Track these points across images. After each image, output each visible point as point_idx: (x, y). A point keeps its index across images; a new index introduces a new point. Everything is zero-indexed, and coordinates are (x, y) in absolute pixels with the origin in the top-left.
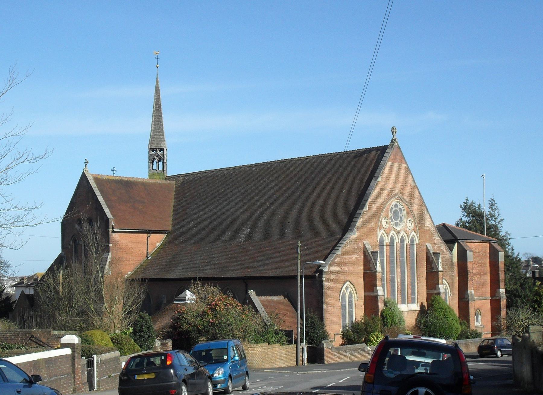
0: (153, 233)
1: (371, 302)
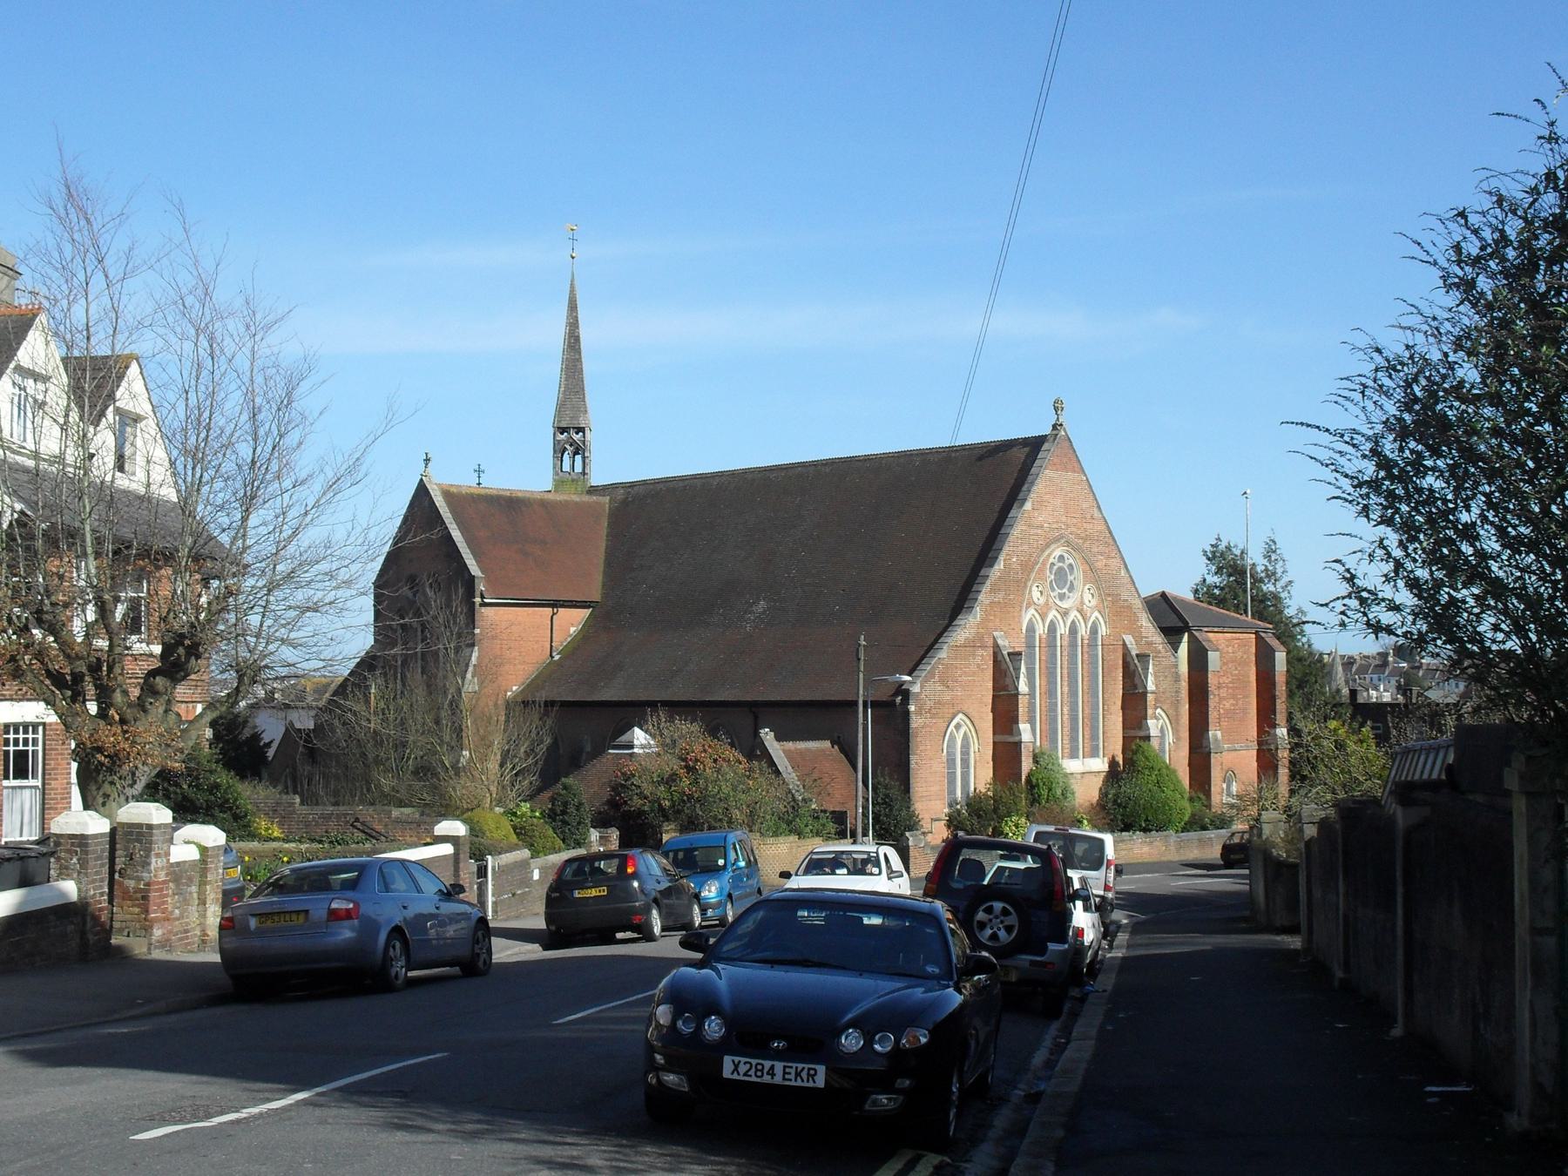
0: (563, 606)
1: (1006, 754)
